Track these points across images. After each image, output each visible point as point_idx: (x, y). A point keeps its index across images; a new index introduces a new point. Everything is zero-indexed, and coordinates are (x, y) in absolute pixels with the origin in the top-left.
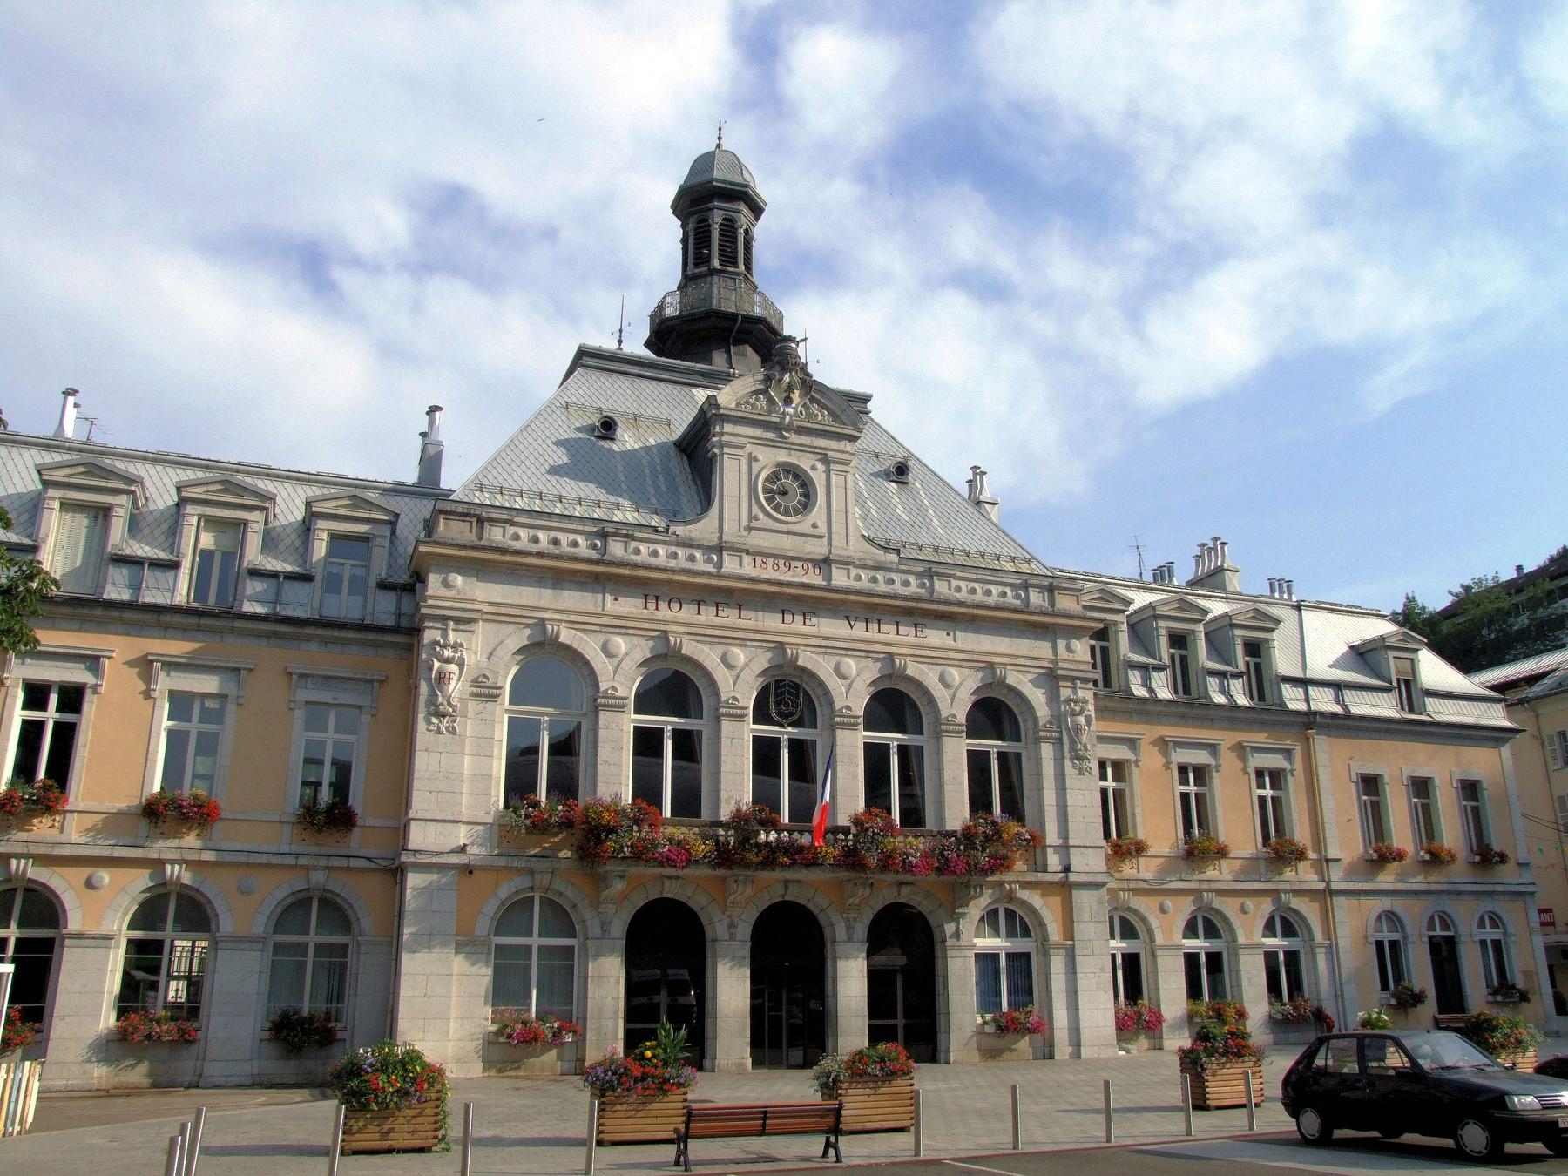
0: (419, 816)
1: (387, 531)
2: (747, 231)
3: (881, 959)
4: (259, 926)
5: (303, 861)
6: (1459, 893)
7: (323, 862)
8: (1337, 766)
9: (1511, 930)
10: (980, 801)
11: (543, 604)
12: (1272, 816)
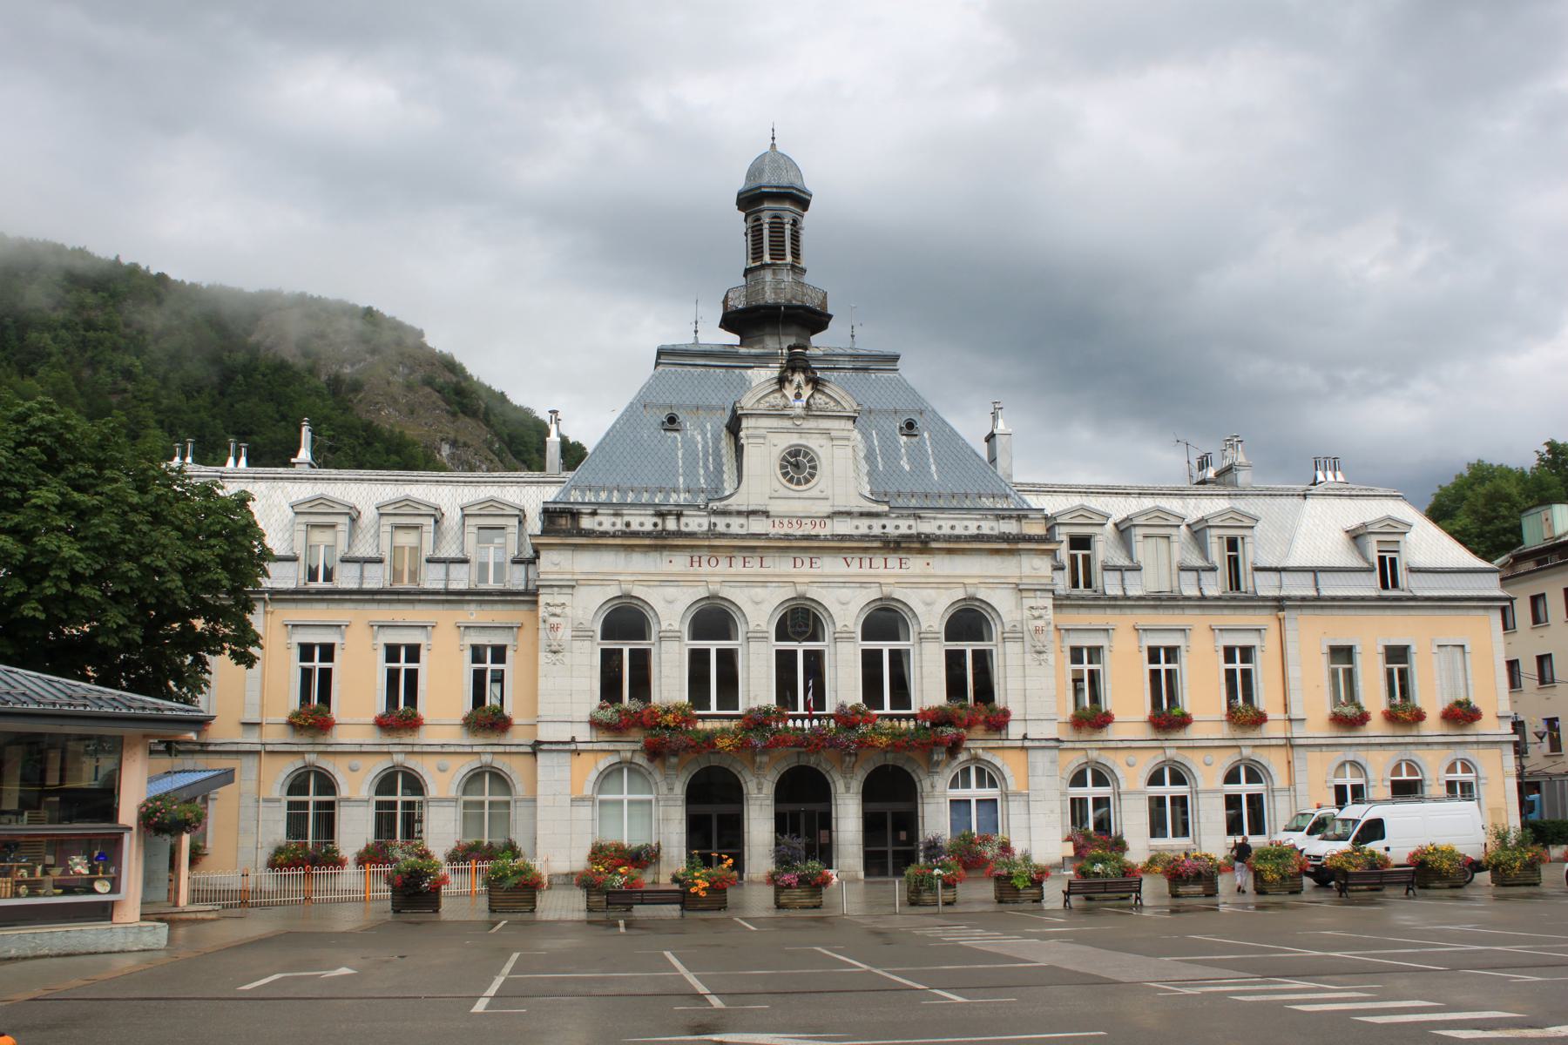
0: (1290, 636)
1: (515, 521)
2: (795, 223)
3: (876, 807)
4: (453, 791)
5: (476, 749)
6: (1428, 744)
7: (489, 749)
8: (1310, 637)
9: (1371, 776)
10: (955, 686)
11: (619, 570)
12: (1239, 686)
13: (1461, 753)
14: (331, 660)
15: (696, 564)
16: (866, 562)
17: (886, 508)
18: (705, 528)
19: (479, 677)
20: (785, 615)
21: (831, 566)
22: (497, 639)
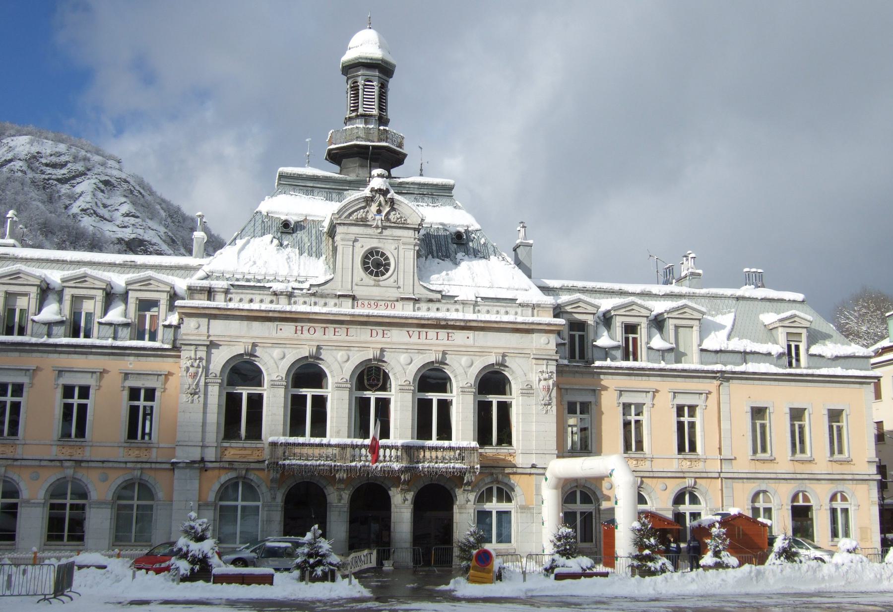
8: (742, 397)
13: (840, 487)
14: (153, 400)
15: (299, 332)
16: (423, 335)
17: (439, 296)
18: (236, 297)
19: (134, 411)
20: (362, 372)
21: (397, 336)
22: (150, 383)
